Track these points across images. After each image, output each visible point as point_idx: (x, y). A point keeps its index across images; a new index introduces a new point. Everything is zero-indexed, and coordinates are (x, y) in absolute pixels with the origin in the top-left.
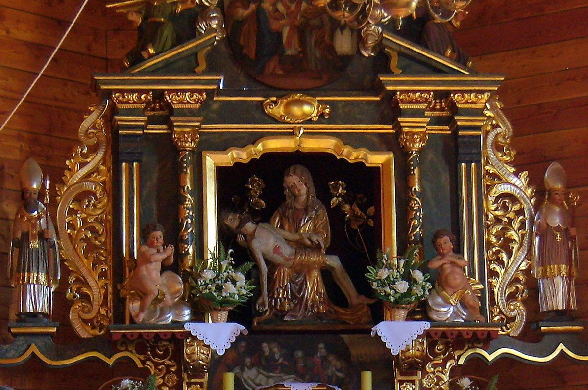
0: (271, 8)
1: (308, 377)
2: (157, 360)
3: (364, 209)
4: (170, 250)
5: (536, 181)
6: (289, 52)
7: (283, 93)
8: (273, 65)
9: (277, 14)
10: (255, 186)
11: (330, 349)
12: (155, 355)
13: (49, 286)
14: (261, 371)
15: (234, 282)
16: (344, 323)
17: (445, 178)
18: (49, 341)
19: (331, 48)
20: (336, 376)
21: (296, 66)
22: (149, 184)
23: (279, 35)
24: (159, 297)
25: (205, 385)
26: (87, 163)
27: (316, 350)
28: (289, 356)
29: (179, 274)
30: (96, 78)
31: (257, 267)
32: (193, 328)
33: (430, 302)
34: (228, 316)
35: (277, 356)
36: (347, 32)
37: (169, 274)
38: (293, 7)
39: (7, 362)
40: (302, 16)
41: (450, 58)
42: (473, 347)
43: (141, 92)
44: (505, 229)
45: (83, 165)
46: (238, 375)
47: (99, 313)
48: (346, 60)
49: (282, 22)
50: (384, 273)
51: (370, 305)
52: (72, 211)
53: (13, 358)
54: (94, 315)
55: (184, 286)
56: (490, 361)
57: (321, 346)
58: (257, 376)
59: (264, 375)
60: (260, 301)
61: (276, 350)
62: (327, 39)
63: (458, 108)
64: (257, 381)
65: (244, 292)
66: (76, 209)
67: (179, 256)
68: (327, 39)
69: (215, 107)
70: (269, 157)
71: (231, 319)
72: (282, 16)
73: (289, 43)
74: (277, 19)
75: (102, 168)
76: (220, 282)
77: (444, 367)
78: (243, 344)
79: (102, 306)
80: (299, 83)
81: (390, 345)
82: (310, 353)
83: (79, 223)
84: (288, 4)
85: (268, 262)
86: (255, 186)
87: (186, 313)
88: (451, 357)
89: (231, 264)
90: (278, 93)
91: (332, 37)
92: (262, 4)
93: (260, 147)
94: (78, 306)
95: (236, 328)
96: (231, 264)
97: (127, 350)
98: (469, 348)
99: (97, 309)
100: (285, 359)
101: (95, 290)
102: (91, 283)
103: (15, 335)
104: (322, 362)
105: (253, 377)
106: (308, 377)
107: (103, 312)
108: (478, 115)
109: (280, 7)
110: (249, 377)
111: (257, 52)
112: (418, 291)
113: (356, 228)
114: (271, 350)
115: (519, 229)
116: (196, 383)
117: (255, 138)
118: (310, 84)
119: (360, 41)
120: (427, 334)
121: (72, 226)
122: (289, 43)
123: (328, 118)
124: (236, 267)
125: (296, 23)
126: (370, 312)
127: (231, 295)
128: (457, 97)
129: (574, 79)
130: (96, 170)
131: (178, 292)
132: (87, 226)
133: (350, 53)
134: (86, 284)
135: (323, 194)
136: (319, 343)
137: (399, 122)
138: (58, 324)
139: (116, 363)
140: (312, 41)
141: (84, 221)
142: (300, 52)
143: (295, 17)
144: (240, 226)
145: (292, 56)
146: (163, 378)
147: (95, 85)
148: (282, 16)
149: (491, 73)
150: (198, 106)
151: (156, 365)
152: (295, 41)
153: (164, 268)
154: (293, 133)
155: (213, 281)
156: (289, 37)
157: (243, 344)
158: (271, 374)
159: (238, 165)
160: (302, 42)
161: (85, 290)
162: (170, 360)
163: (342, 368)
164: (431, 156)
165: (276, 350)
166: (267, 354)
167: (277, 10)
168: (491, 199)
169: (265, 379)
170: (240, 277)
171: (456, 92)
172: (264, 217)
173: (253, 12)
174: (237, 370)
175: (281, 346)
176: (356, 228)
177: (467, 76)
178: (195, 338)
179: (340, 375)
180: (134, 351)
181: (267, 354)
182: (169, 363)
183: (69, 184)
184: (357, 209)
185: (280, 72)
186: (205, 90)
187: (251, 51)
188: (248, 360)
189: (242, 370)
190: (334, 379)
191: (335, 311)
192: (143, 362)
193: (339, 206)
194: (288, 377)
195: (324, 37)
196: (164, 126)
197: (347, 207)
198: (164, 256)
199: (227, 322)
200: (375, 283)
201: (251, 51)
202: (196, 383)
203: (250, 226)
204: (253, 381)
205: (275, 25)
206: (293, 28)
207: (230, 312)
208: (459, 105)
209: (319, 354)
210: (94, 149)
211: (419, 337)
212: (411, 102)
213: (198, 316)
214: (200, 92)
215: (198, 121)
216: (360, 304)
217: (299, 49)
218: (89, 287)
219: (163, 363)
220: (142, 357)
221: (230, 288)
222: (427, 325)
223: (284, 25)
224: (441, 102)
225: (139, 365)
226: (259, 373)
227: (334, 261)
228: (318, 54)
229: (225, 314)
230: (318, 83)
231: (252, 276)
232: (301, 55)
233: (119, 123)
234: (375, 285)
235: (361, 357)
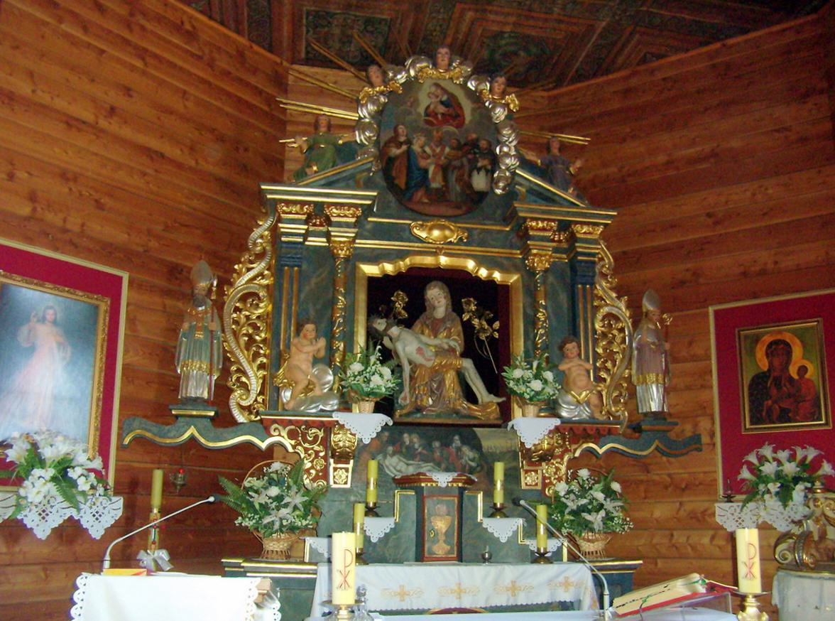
0: (419, 150)
1: (443, 466)
2: (307, 445)
3: (490, 323)
4: (322, 343)
5: (634, 306)
6: (435, 185)
7: (427, 218)
8: (419, 195)
9: (425, 154)
10: (400, 301)
11: (464, 442)
12: (305, 441)
13: (211, 374)
14: (402, 458)
15: (381, 375)
16: (476, 418)
17: (563, 298)
18: (207, 423)
19: (470, 186)
20: (469, 464)
21: (440, 197)
22: (307, 288)
23: (426, 171)
24: (286, 268)
25: (350, 470)
26: (253, 268)
27: (452, 441)
28: (428, 446)
29: (330, 367)
30: (263, 187)
31: (399, 366)
32: (339, 417)
33: (560, 401)
34: (375, 407)
35: (416, 446)
36: (482, 173)
37: (321, 366)
38: (438, 150)
39: (168, 441)
40: (445, 158)
41: (572, 195)
42: (588, 442)
43: (303, 203)
44: (610, 343)
45: (249, 270)
46: (381, 462)
47: (256, 400)
48: (482, 196)
49: (429, 161)
50: (517, 373)
51: (499, 404)
52: (237, 310)
53: (175, 437)
54: (252, 402)
55: (334, 378)
56: (600, 453)
57: (457, 437)
58: (397, 464)
59: (406, 463)
60: (402, 395)
61: (415, 440)
62: (466, 177)
63: (577, 237)
64: (398, 468)
65: (390, 385)
66: (241, 307)
67: (330, 349)
68: (466, 177)
69: (369, 227)
70: (413, 270)
71: (378, 409)
72: (428, 157)
73: (434, 178)
74: (423, 158)
75: (266, 272)
76: (368, 375)
77: (562, 459)
78: (386, 434)
79: (259, 395)
80: (443, 210)
81: (524, 438)
82: (446, 444)
83: (243, 320)
84: (434, 147)
85: (410, 363)
86: (400, 301)
87: (334, 403)
88: (567, 451)
89: (378, 359)
90: (424, 218)
91: (470, 176)
92: (412, 146)
93: (408, 261)
94: (238, 393)
95: (382, 419)
96: (378, 359)
97: (280, 435)
98: (583, 443)
99: (255, 397)
100: (423, 449)
101: (253, 380)
102: (250, 373)
103: (177, 417)
104: (457, 452)
105: (394, 464)
106: (443, 466)
107: (260, 399)
108: (596, 244)
109: (427, 149)
110: (390, 464)
111: (407, 184)
112: (549, 390)
113: (484, 339)
114: (411, 441)
115: (621, 343)
116: (341, 468)
117: (402, 255)
118: (450, 212)
119: (493, 182)
120: (557, 429)
121: (236, 322)
122: (434, 178)
123: (501, 195)
124: (382, 362)
125: (441, 163)
126: (498, 410)
127: (379, 387)
128: (578, 227)
129: (654, 231)
130: (261, 275)
131: (328, 383)
132: (249, 322)
133: (485, 190)
134: (245, 373)
135: (457, 308)
136: (454, 436)
137: (529, 245)
138: (215, 408)
139: (606, 452)
140: (453, 178)
141: (247, 317)
142: (443, 186)
143: (440, 158)
144: (386, 329)
145: (437, 190)
146: (312, 462)
147: (261, 193)
148: (428, 157)
149: (608, 209)
150: (353, 220)
151: (306, 450)
152: (439, 178)
153: (316, 361)
154: (436, 252)
155: (360, 373)
156: (434, 173)
157: (386, 434)
158: (411, 462)
159: (386, 277)
160: (445, 178)
161: (244, 379)
162: (318, 445)
163: (474, 458)
164: (551, 279)
165: (415, 440)
166: (408, 443)
167: (425, 152)
168: (599, 316)
169: (405, 466)
170: (386, 371)
171: (577, 223)
172: (408, 324)
173: (403, 153)
174: (380, 457)
175: (421, 437)
176: (484, 339)
177: (583, 208)
178: (342, 427)
179: (473, 464)
180: (286, 437)
181: (408, 443)
182: (316, 448)
183: (236, 286)
184: (484, 323)
185: (426, 201)
186: (362, 205)
187: (401, 182)
188: (390, 449)
189: (385, 457)
190: (467, 468)
191: (469, 408)
192: (294, 447)
193: (469, 321)
194: (426, 464)
195: (463, 175)
196: (324, 240)
197: (477, 320)
198: (316, 348)
199: (374, 412)
200: (512, 382)
201: (401, 182)
202: (341, 468)
203: (395, 331)
204: (395, 468)
205: (423, 163)
206: (437, 165)
207: (377, 403)
208: (578, 235)
209: (454, 445)
210: (260, 256)
211: (550, 432)
212: (539, 229)
213: (346, 407)
214: (356, 206)
215: (353, 233)
216: (490, 402)
217: (443, 184)
218: (248, 378)
219: (312, 449)
220: (293, 442)
221: (376, 380)
222: (557, 422)
223: (430, 164)
224: (559, 235)
225: (291, 450)
226: (400, 460)
227: (468, 364)
228: (458, 188)
229: (369, 406)
230: (459, 212)
231: (397, 371)
232: (444, 189)
233: (282, 230)
234: (511, 384)
235: (491, 448)
